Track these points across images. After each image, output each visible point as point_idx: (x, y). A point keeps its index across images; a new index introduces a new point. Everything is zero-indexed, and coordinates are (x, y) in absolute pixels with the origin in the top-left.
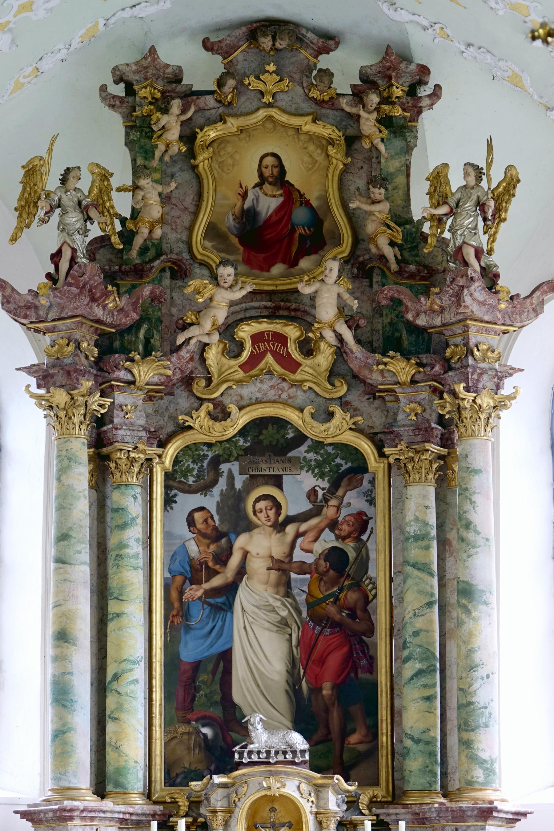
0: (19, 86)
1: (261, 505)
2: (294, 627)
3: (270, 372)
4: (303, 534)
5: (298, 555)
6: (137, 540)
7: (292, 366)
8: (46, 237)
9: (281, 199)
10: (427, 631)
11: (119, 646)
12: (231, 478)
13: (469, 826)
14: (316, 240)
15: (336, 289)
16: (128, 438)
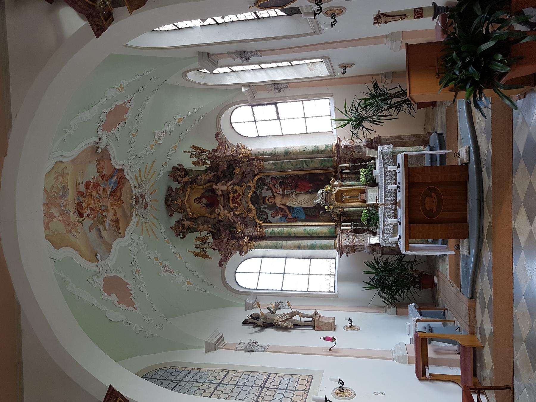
0: (180, 257)
5: (281, 192)
7: (239, 194)
8: (210, 252)
11: (302, 233)
14: (213, 191)
15: (220, 186)
16: (255, 232)
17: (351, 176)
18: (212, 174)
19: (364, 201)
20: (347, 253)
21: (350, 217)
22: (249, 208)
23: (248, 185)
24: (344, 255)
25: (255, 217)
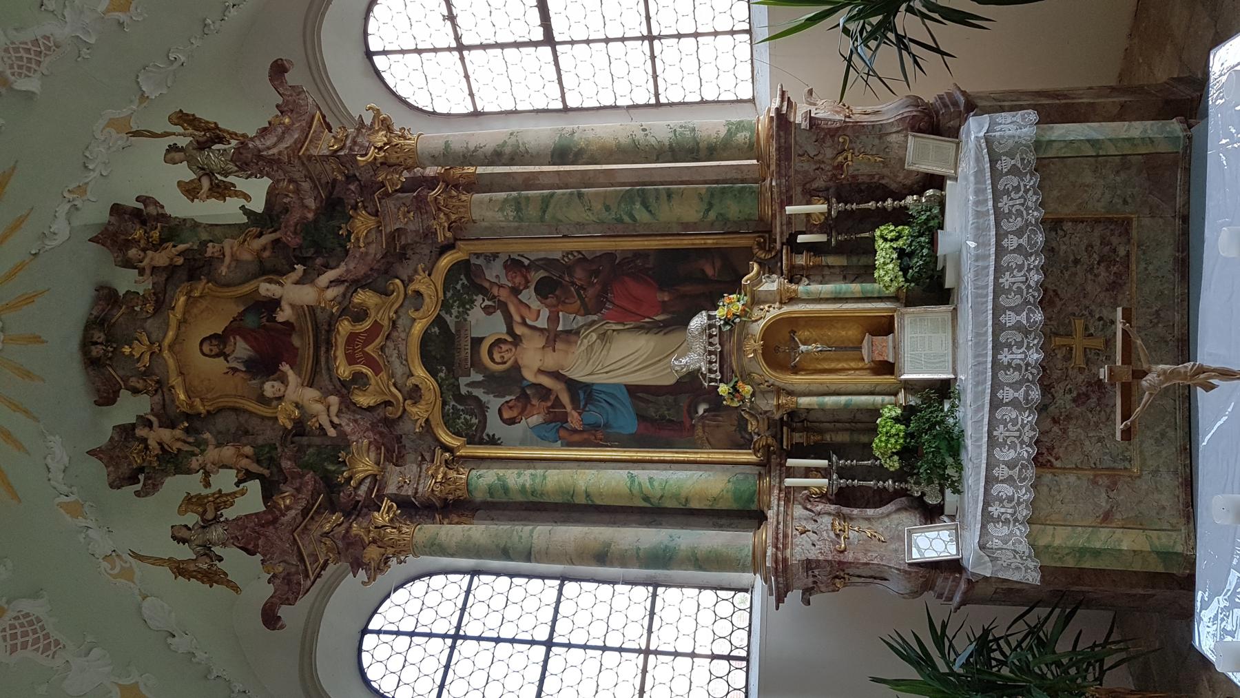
1: (497, 357)
2: (605, 327)
3: (382, 349)
4: (523, 319)
5: (542, 323)
6: (519, 475)
7: (377, 326)
8: (233, 560)
9: (238, 337)
10: (605, 197)
12: (472, 384)
13: (796, 142)
17: (831, 260)
18: (265, 240)
19: (887, 368)
20: (808, 592)
21: (821, 432)
22: (413, 380)
23: (412, 287)
24: (794, 596)
25: (437, 419)
